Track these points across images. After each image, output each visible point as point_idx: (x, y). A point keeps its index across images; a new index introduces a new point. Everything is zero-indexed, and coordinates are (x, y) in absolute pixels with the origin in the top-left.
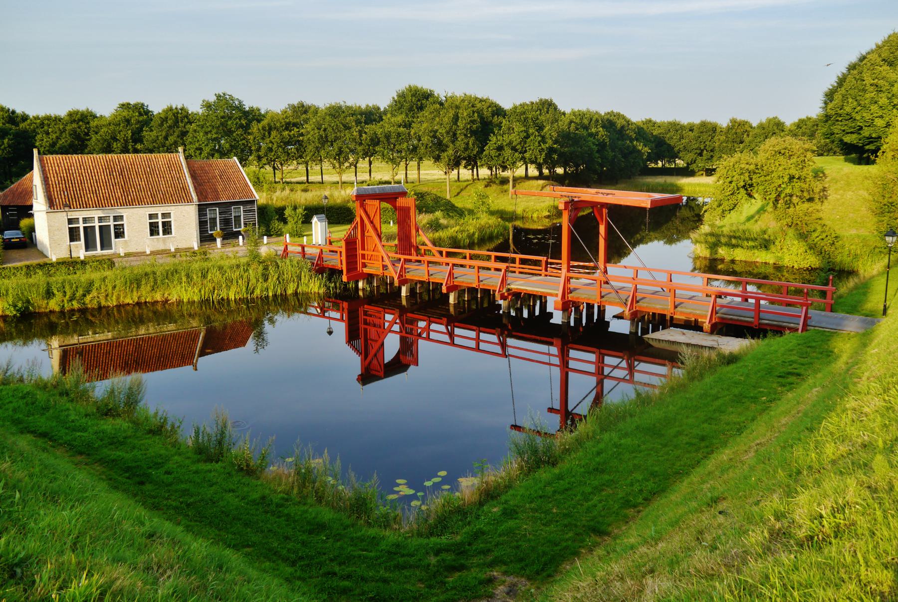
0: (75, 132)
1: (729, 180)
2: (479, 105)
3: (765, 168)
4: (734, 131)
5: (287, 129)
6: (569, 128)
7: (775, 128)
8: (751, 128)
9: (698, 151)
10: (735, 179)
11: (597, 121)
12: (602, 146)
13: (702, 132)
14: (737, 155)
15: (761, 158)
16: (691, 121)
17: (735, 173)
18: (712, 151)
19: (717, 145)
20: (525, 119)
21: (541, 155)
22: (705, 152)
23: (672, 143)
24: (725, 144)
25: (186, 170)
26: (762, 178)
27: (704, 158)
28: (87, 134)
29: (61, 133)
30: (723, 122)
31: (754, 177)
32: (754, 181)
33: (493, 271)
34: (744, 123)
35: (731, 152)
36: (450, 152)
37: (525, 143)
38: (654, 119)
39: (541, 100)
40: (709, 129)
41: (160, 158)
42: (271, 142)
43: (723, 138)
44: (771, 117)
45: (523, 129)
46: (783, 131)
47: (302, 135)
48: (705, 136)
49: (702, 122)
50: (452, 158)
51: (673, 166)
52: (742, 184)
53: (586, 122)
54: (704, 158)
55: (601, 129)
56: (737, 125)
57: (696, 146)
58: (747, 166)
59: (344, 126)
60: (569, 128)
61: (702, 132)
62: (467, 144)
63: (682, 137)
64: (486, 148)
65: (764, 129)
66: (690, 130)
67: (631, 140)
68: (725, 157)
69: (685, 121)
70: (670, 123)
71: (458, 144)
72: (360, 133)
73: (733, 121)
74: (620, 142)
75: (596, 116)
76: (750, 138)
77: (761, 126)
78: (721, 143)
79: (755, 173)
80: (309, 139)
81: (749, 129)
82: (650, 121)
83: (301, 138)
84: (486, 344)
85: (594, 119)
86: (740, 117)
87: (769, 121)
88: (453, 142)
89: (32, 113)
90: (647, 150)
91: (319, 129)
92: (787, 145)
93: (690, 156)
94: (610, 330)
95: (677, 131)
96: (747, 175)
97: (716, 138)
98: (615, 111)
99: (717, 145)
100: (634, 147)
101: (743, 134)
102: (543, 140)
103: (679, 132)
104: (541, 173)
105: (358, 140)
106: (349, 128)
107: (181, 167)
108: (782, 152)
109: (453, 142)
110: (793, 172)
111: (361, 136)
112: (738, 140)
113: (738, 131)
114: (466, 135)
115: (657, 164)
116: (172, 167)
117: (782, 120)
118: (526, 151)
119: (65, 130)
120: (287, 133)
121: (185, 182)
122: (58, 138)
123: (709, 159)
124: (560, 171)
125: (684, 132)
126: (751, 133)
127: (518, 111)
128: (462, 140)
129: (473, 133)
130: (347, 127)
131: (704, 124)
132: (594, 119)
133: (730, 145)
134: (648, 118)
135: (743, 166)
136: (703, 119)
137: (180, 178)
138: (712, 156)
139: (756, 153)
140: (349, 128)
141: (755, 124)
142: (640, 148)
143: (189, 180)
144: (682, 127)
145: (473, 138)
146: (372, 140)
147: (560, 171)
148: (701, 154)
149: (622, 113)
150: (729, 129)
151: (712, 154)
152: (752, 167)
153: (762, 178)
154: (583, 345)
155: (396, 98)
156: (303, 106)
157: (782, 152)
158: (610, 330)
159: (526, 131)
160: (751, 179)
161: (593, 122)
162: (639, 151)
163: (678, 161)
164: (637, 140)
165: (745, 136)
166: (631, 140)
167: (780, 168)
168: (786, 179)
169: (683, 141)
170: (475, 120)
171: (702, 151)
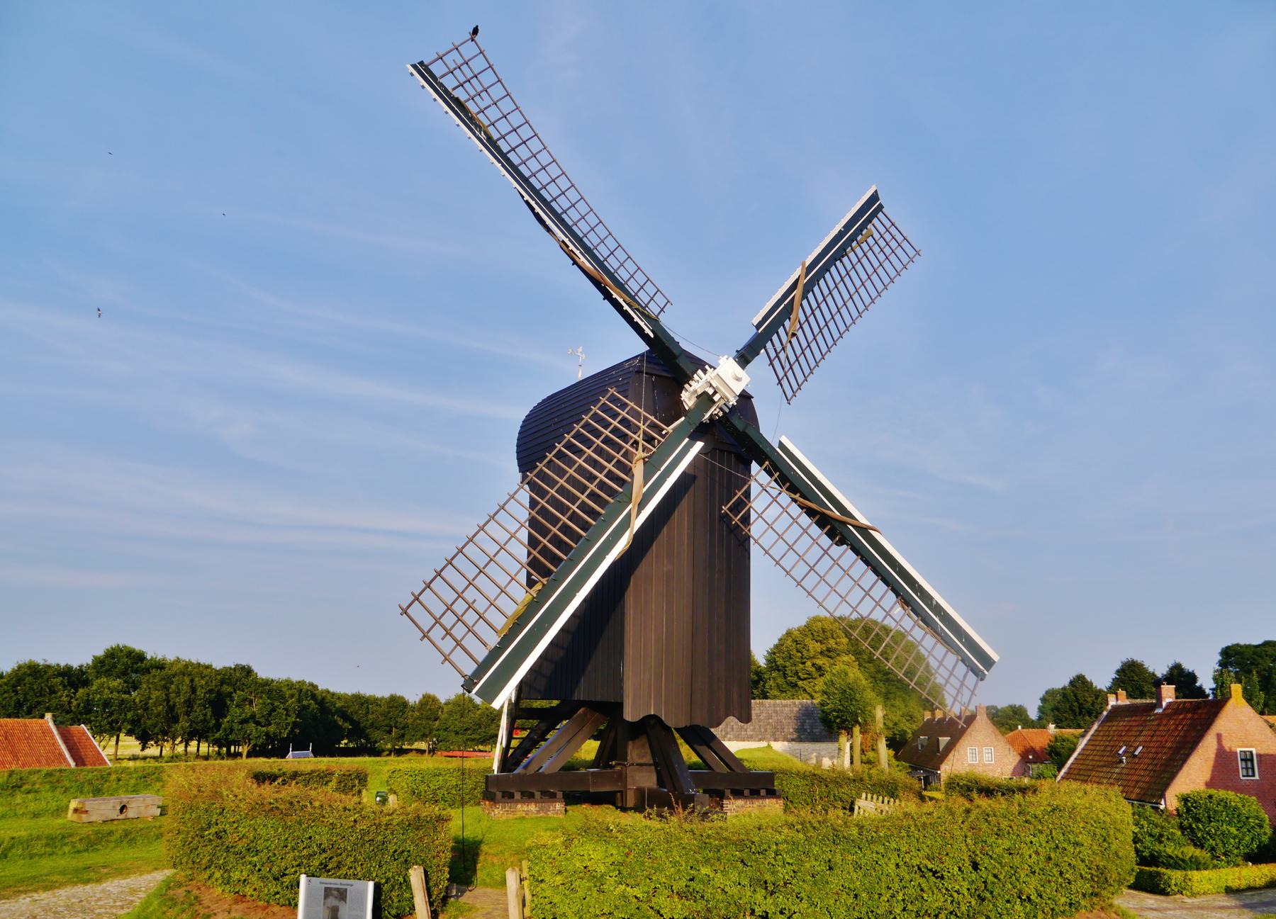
9: (388, 729)
13: (391, 707)
18: (403, 728)
19: (410, 721)
25: (58, 737)
33: (458, 758)
40: (397, 704)
41: (33, 723)
48: (393, 713)
49: (392, 695)
61: (391, 707)
71: (193, 715)
78: (415, 720)
84: (885, 224)
88: (187, 713)
94: (648, 348)
95: (362, 704)
100: (335, 722)
103: (365, 705)
107: (52, 732)
109: (187, 713)
111: (70, 703)
112: (433, 717)
114: (204, 706)
124: (258, 748)
129: (211, 702)
131: (393, 699)
137: (55, 743)
142: (341, 723)
146: (85, 708)
154: (578, 565)
155: (417, 703)
158: (648, 348)
162: (340, 727)
165: (440, 713)
171: (391, 727)
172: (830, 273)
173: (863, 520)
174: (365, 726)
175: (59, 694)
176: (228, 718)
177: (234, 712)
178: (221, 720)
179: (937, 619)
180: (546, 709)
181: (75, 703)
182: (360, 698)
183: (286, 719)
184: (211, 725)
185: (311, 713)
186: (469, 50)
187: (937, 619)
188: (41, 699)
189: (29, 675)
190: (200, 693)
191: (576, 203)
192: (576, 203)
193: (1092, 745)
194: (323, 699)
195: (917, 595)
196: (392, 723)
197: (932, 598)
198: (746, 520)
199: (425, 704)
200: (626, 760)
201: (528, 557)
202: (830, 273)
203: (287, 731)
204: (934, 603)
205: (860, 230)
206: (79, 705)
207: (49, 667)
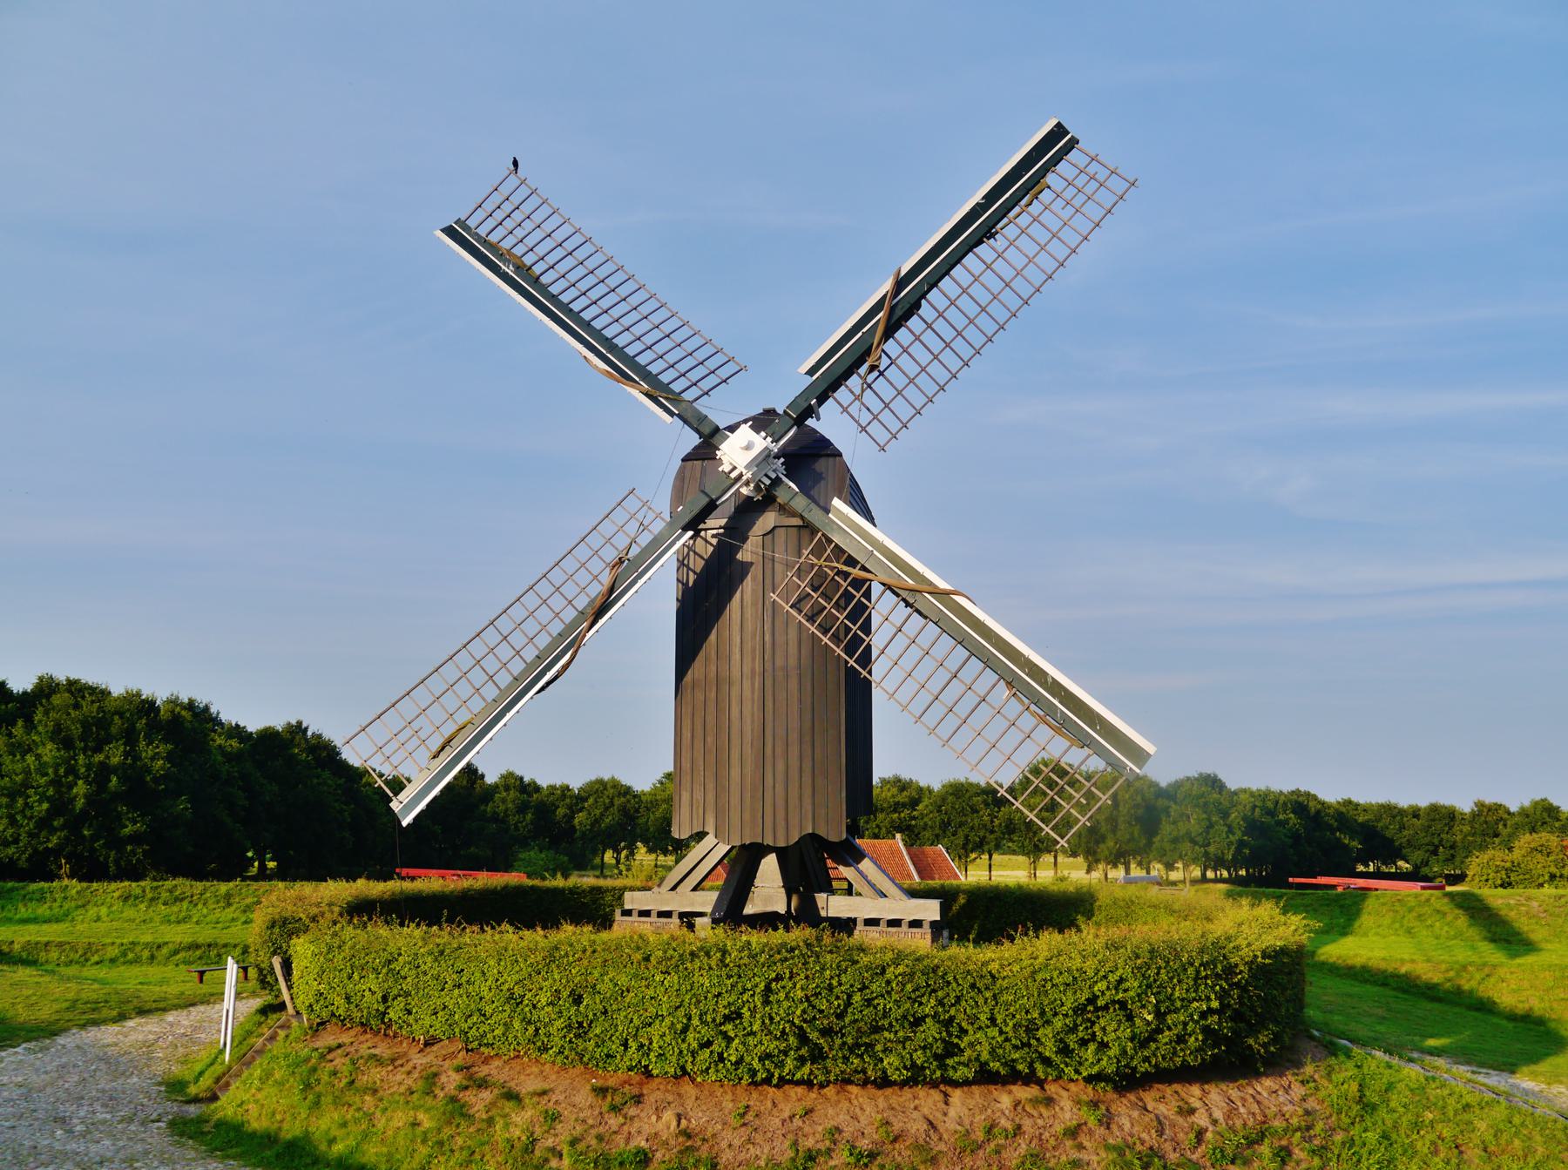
0: (625, 807)
1: (1485, 877)
2: (1137, 784)
3: (1522, 866)
4: (1483, 818)
5: (895, 811)
6: (1253, 814)
7: (1545, 815)
8: (1509, 813)
9: (1431, 848)
10: (1490, 877)
11: (1285, 804)
12: (1296, 837)
13: (1434, 820)
14: (1490, 852)
15: (1517, 855)
16: (1413, 802)
17: (1490, 871)
19: (1459, 838)
20: (1206, 804)
21: (1229, 849)
22: (1441, 849)
23: (1388, 834)
24: (1470, 838)
26: (1521, 877)
27: (1441, 858)
28: (637, 811)
29: (607, 809)
30: (1465, 806)
31: (1512, 875)
32: (1512, 878)
34: (1497, 807)
35: (1483, 847)
36: (1110, 844)
37: (1208, 833)
38: (1355, 799)
39: (1201, 774)
40: (1443, 817)
42: (878, 826)
43: (1467, 829)
44: (1538, 798)
45: (1204, 816)
46: (1558, 820)
47: (914, 818)
49: (1432, 805)
50: (1114, 852)
51: (1393, 870)
52: (1499, 882)
53: (1270, 805)
54: (1441, 858)
55: (1292, 816)
56: (1485, 810)
57: (1427, 840)
58: (1503, 864)
59: (971, 807)
60: (1253, 814)
61: (1434, 820)
62: (1132, 834)
63: (1402, 827)
64: (1157, 839)
65: (1528, 816)
66: (1414, 817)
67: (1333, 831)
68: (1478, 854)
69: (1404, 802)
70: (1382, 806)
72: (993, 817)
73: (1480, 805)
74: (1317, 834)
75: (1283, 798)
76: (1509, 830)
77: (1524, 812)
78: (1465, 836)
79: (1512, 871)
80: (926, 824)
81: (1506, 816)
82: (1350, 802)
83: (913, 822)
85: (1281, 802)
86: (1489, 799)
87: (1536, 804)
89: (544, 782)
90: (1355, 844)
91: (939, 811)
92: (1543, 841)
93: (1418, 856)
95: (1394, 817)
96: (1503, 872)
97: (1456, 828)
98: (1302, 789)
99: (1459, 838)
100: (1339, 840)
101: (1497, 824)
102: (1230, 830)
103: (1398, 818)
104: (1204, 875)
105: (989, 826)
106: (977, 812)
108: (1539, 849)
110: (1553, 870)
111: (992, 822)
112: (1491, 832)
113: (1489, 819)
114: (1129, 823)
115: (1368, 866)
116: (895, 852)
117: (1555, 803)
118: (1208, 844)
119: (612, 804)
120: (896, 815)
121: (909, 870)
122: (602, 815)
123: (1447, 860)
125: (1405, 819)
126: (1509, 823)
127: (1194, 793)
128: (51, 751)
129: (1138, 819)
130: (975, 811)
131: (1434, 809)
132: (1281, 802)
133: (1479, 840)
134: (1346, 798)
135: (1498, 863)
136: (1433, 801)
137: (904, 864)
138: (1453, 856)
139: (1510, 849)
140: (977, 812)
141: (1514, 808)
142: (1346, 842)
143: (912, 868)
144: (1402, 812)
145: (1138, 827)
146: (1007, 827)
147: (1243, 872)
148: (1435, 853)
149: (1312, 792)
150: (1475, 816)
151: (1452, 852)
152: (1508, 865)
153: (1521, 877)
156: (899, 781)
157: (1539, 849)
159: (1209, 819)
160: (1509, 877)
161: (1280, 805)
162: (1346, 846)
163: (1401, 863)
164: (1339, 829)
165: (1501, 827)
166: (1333, 831)
167: (1539, 866)
168: (1547, 878)
169: (1405, 833)
170: (1138, 805)
171: (1437, 847)
172: (671, 383)
173: (942, 584)
174: (1401, 844)
175: (981, 813)
176: (1158, 838)
177: (1166, 829)
178: (268, 872)
179: (1056, 702)
180: (186, 875)
181: (997, 822)
182: (1390, 809)
183: (1228, 837)
184: (1141, 845)
185: (1290, 830)
186: (1117, 185)
187: (1056, 702)
188: (964, 819)
189: (951, 794)
190: (1123, 809)
191: (944, 318)
192: (944, 318)
193: (86, 954)
194: (1318, 812)
195: (1024, 672)
196: (1436, 841)
197: (1045, 674)
198: (867, 628)
199: (1478, 815)
200: (500, 925)
201: (871, 669)
202: (671, 383)
203: (1231, 852)
204: (1050, 680)
205: (1026, 189)
206: (1000, 824)
207: (971, 784)
